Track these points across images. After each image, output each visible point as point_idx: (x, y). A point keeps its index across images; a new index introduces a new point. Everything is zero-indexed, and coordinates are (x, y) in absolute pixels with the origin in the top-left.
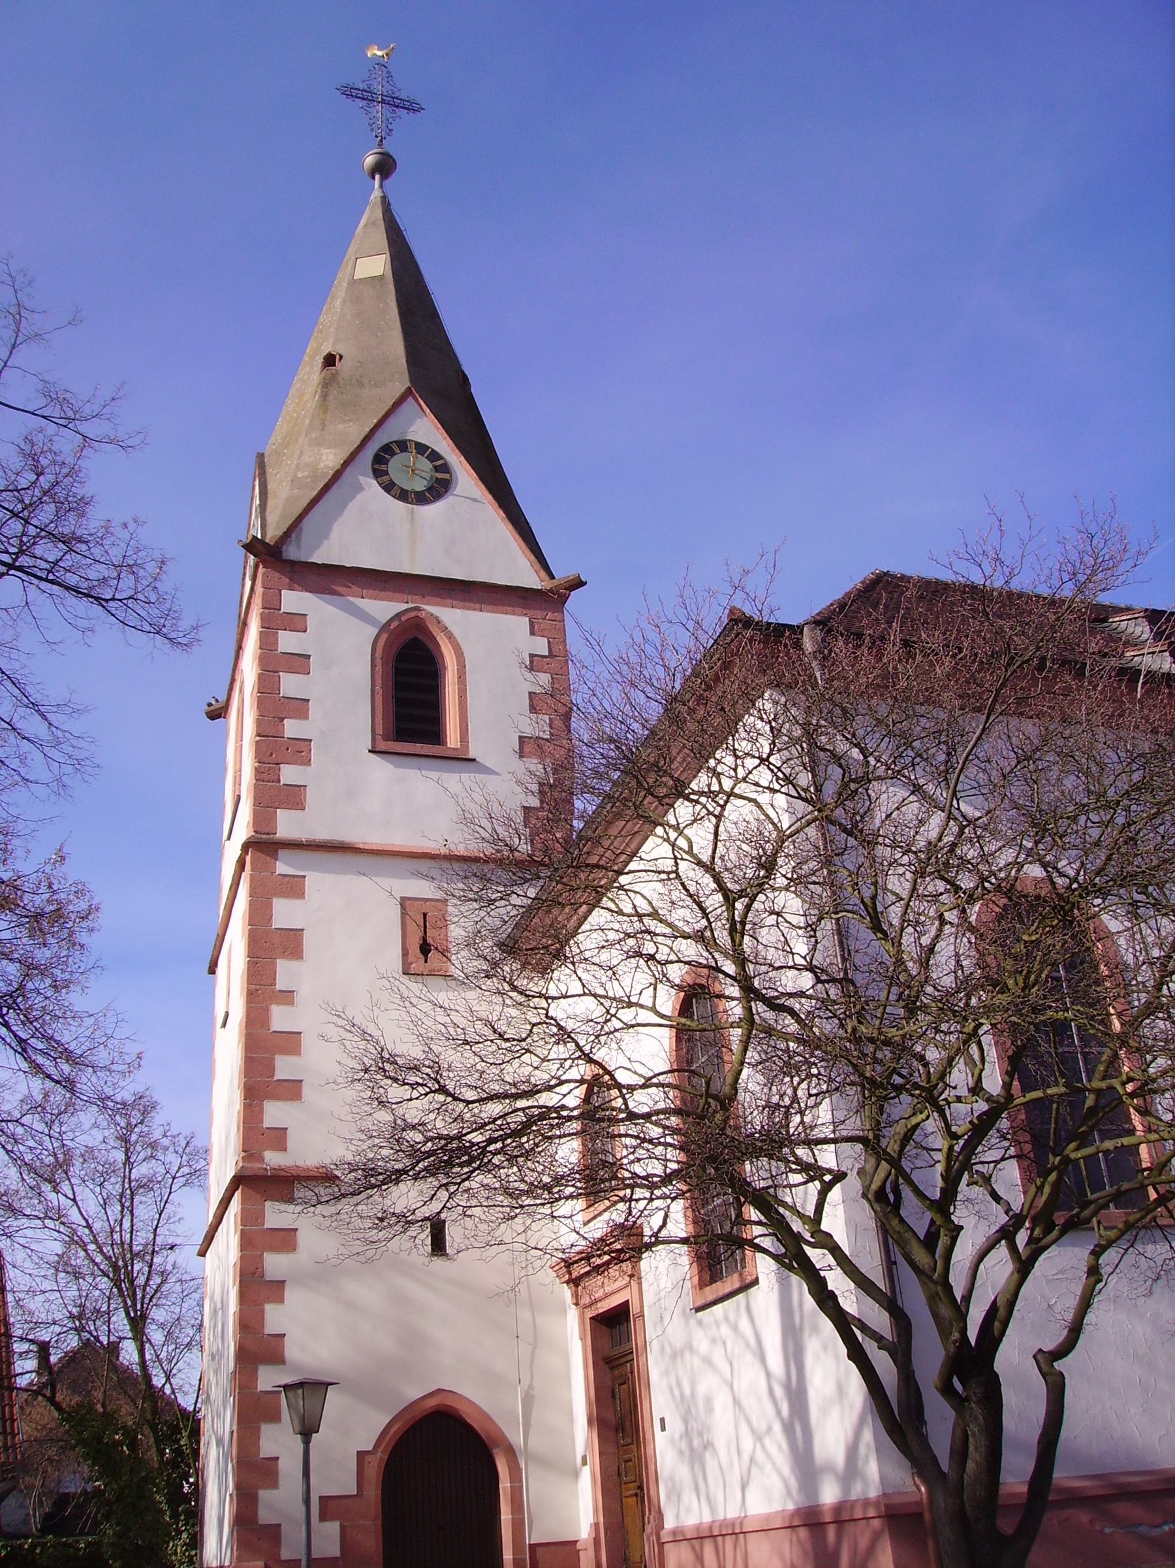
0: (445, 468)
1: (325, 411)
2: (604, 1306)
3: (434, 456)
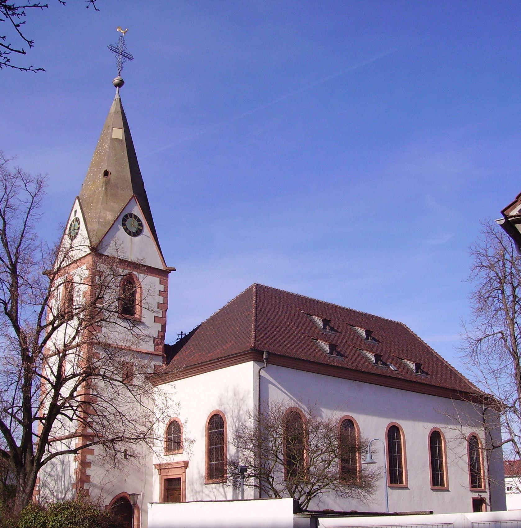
0: (141, 225)
1: (107, 196)
2: (169, 477)
3: (139, 220)
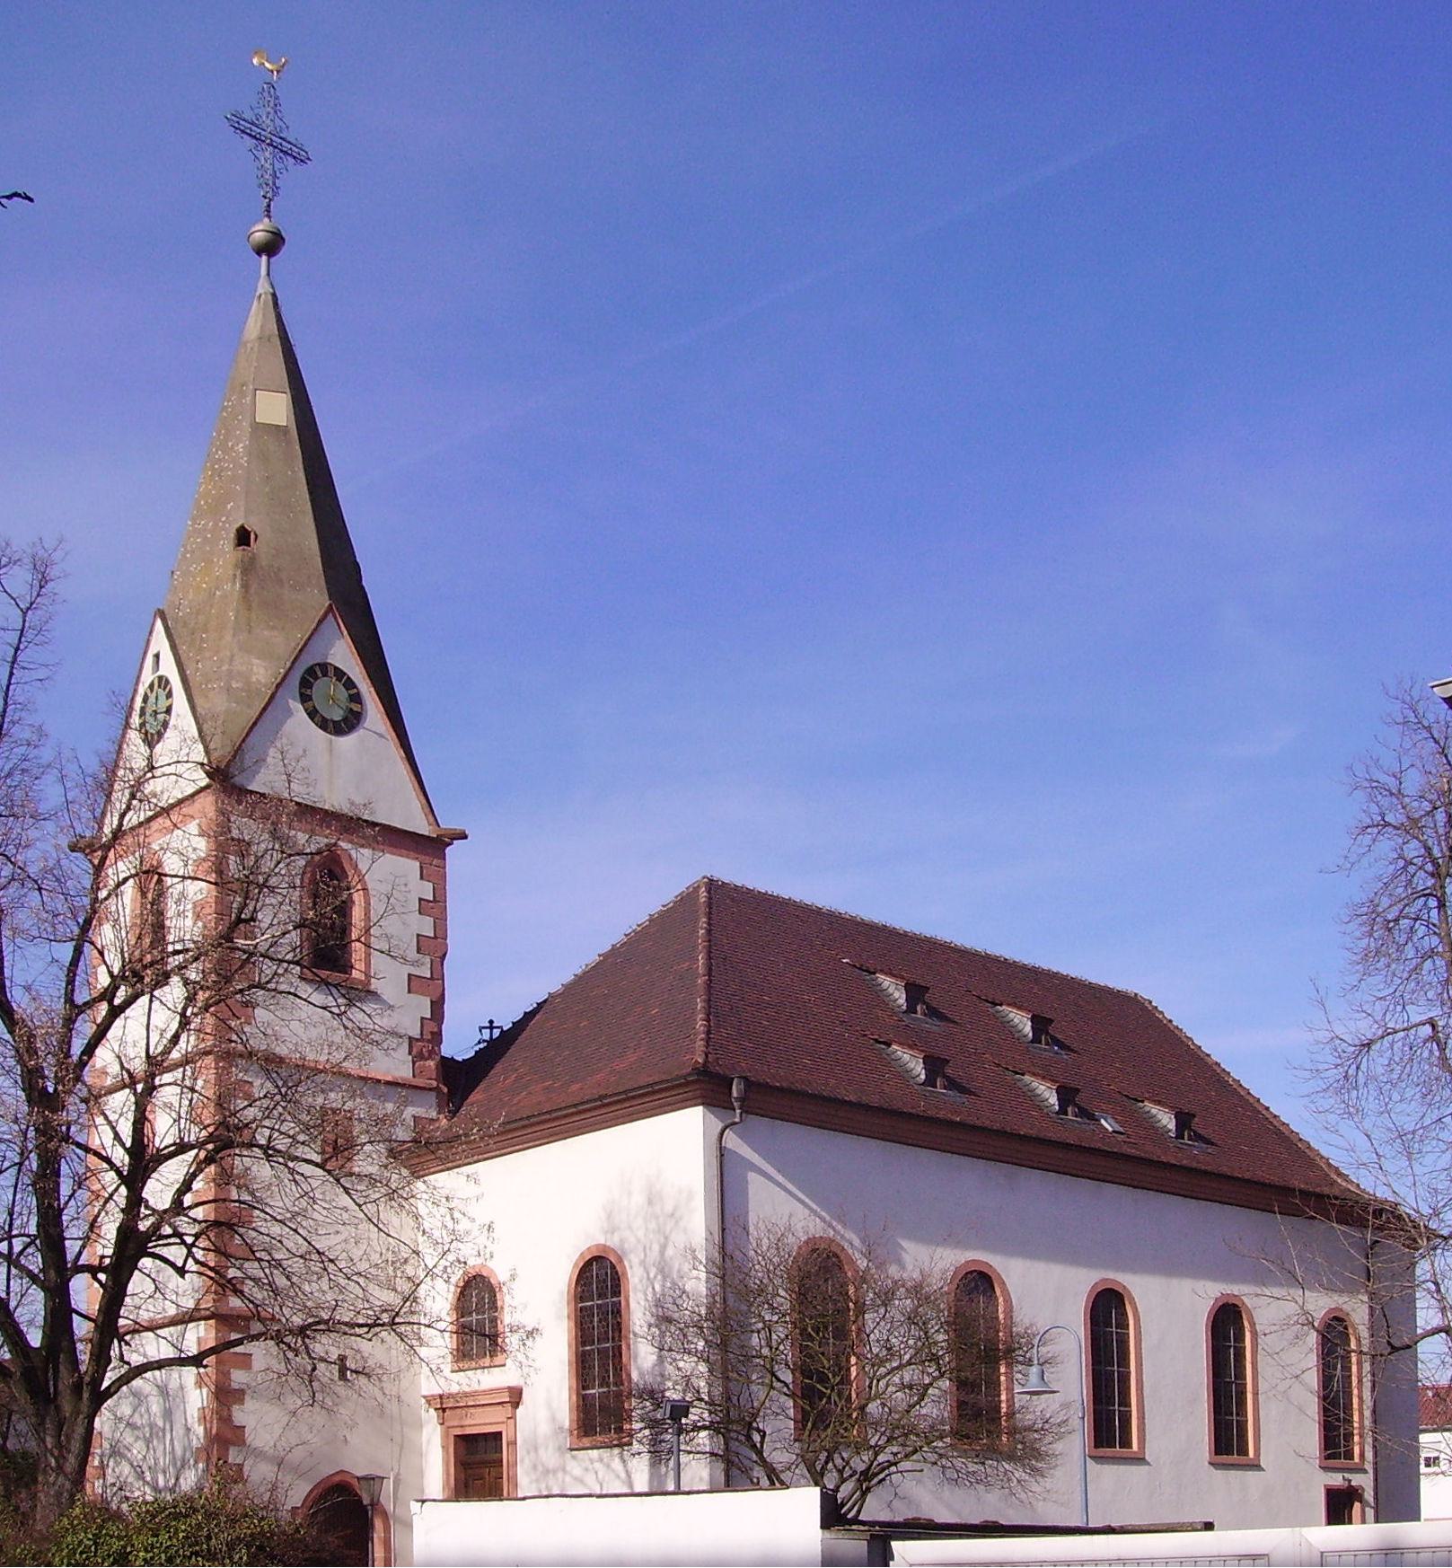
0: (356, 698)
1: (249, 609)
3: (350, 684)
